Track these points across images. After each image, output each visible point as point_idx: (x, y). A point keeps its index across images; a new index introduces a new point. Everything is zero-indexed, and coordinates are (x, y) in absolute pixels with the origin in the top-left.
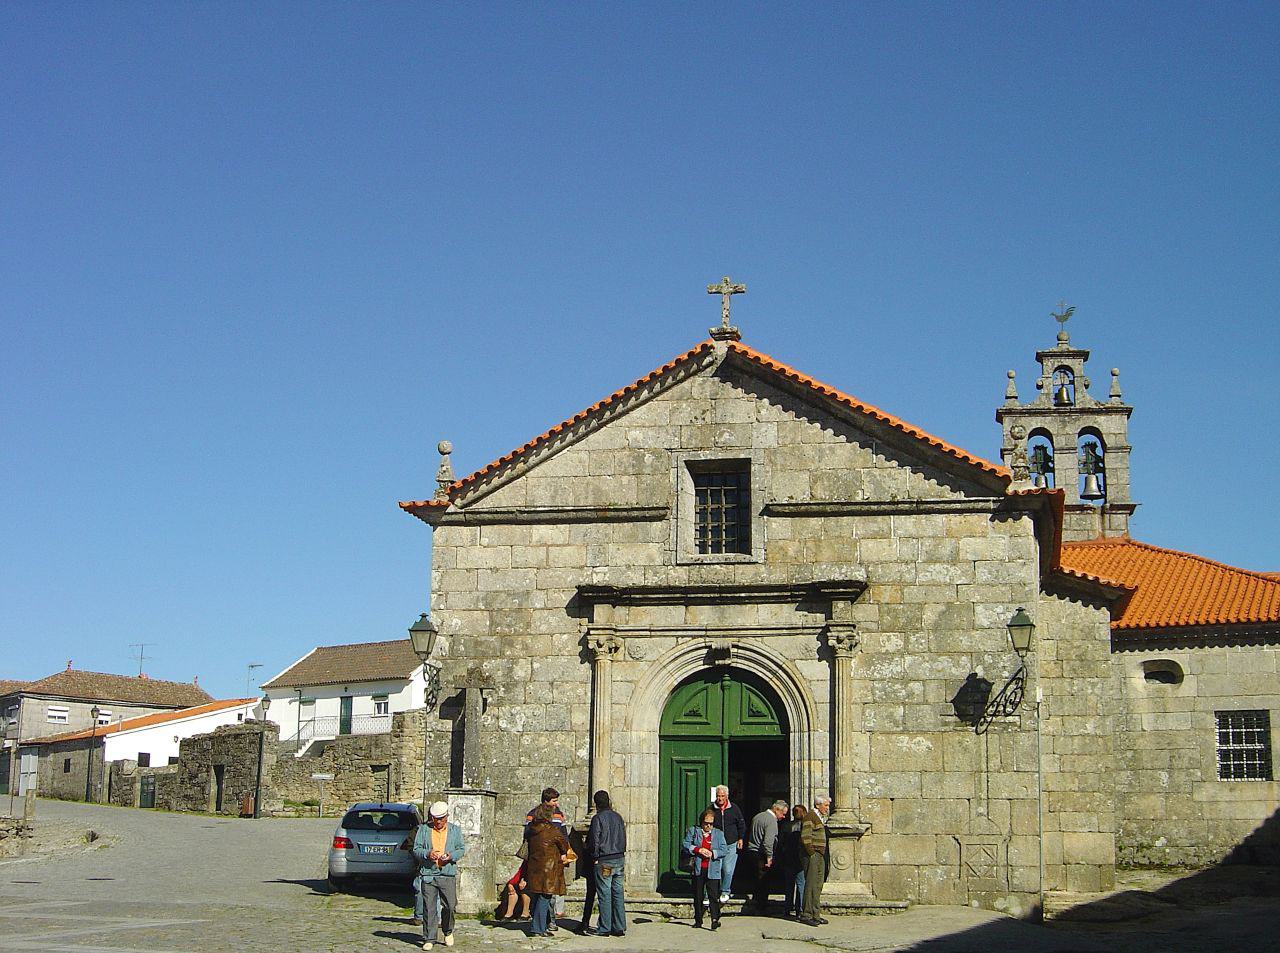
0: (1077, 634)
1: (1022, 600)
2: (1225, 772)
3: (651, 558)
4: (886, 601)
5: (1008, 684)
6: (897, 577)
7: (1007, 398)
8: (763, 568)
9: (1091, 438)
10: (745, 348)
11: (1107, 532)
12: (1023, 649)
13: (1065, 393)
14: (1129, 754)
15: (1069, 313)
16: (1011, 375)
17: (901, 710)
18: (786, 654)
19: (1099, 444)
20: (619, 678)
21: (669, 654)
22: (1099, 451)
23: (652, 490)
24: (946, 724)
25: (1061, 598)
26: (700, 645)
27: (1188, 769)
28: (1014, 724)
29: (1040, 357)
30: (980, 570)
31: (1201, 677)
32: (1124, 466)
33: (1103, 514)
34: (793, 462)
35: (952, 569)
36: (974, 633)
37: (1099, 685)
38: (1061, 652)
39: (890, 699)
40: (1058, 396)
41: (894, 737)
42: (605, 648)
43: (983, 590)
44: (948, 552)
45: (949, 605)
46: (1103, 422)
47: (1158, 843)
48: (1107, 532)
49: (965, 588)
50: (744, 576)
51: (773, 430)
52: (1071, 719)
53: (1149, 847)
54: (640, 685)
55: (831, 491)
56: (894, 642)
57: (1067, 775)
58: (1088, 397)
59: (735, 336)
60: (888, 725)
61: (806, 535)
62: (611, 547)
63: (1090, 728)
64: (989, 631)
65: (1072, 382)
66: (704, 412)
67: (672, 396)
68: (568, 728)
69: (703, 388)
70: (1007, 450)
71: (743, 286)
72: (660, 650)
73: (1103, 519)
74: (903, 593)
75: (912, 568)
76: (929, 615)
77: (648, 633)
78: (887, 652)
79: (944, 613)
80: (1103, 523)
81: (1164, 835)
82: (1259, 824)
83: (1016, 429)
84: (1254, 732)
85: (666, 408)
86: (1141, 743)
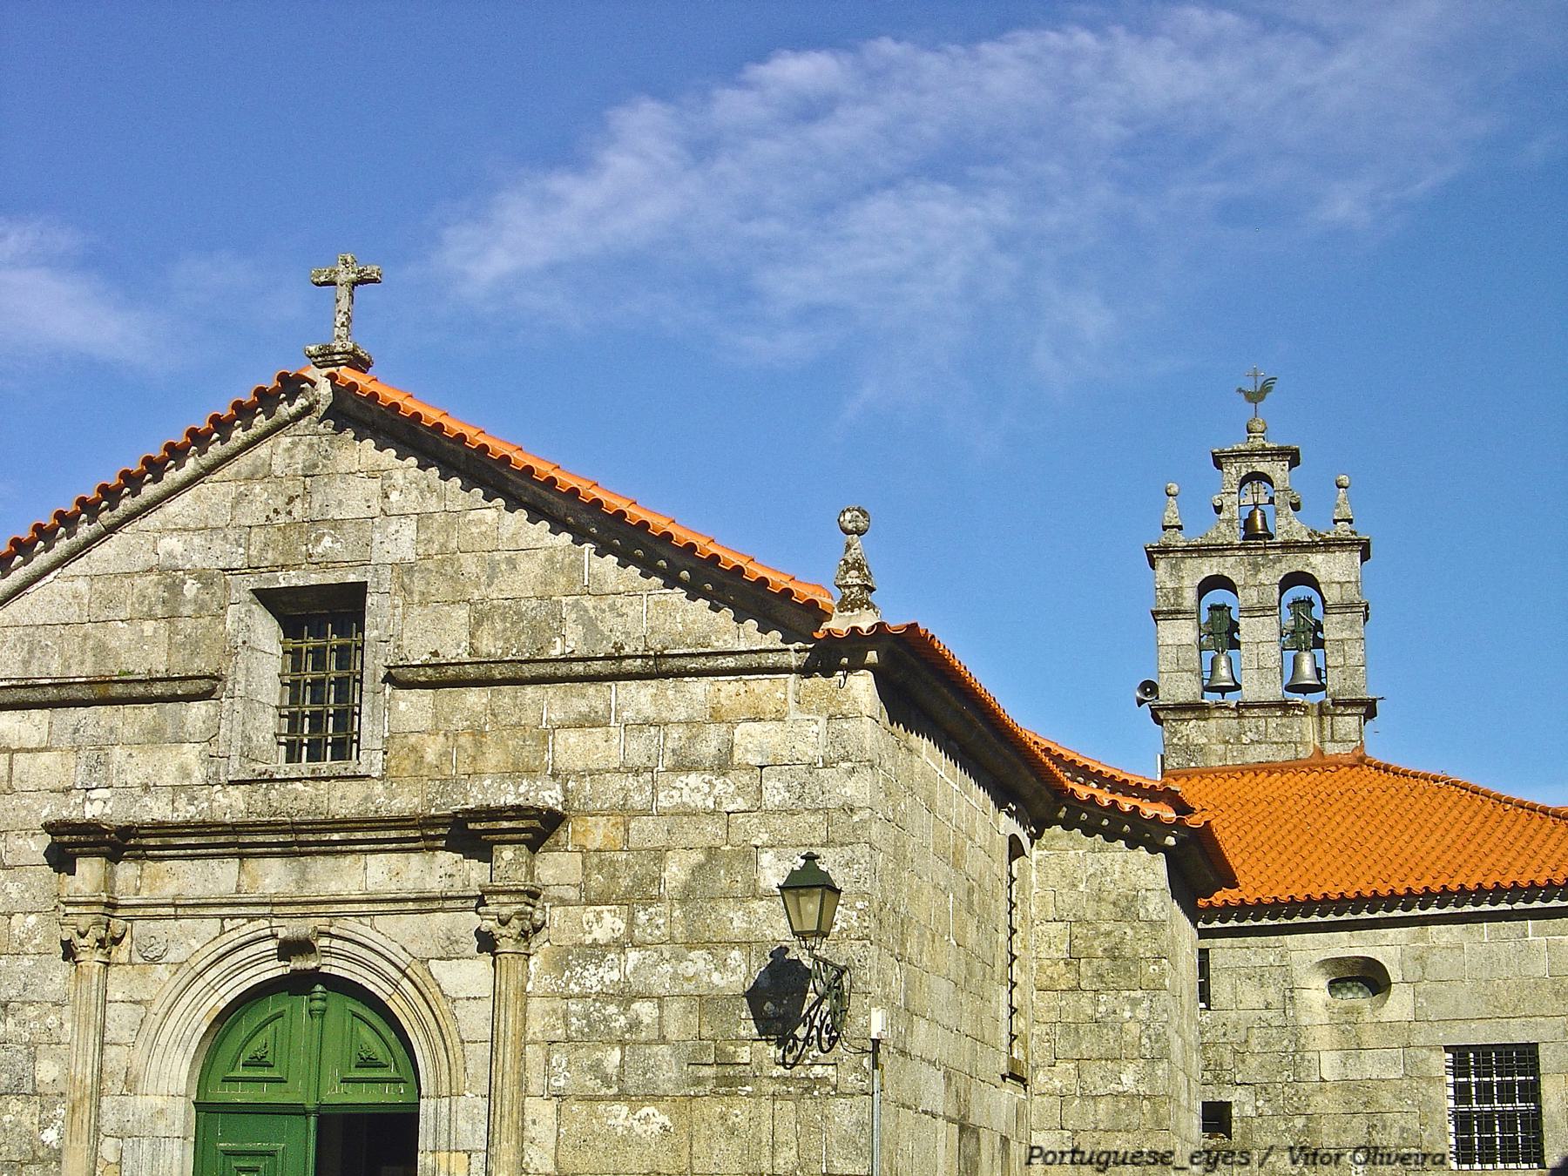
0: (1106, 910)
1: (848, 840)
3: (185, 772)
4: (596, 845)
6: (617, 799)
8: (379, 787)
10: (373, 387)
11: (1328, 746)
13: (1259, 518)
14: (1299, 1122)
15: (1266, 389)
16: (1171, 491)
17: (615, 1055)
18: (412, 948)
19: (1316, 599)
20: (119, 996)
21: (206, 951)
22: (1317, 612)
23: (194, 646)
24: (699, 1081)
26: (262, 933)
29: (1218, 461)
30: (770, 784)
31: (1421, 987)
32: (1355, 636)
34: (441, 589)
35: (719, 785)
36: (755, 904)
37: (1146, 1004)
38: (1077, 942)
39: (595, 1033)
40: (1249, 524)
41: (601, 1106)
42: (89, 940)
43: (777, 822)
44: (714, 751)
45: (712, 852)
46: (1320, 564)
48: (1328, 746)
49: (741, 818)
50: (344, 800)
51: (409, 530)
52: (1092, 1067)
54: (155, 1009)
55: (507, 640)
56: (608, 924)
58: (1296, 524)
59: (359, 363)
60: (592, 1084)
61: (459, 723)
62: (118, 754)
63: (1128, 1080)
65: (1272, 501)
66: (291, 500)
67: (238, 472)
68: (28, 1088)
69: (291, 457)
71: (372, 270)
72: (193, 942)
73: (1321, 720)
74: (627, 830)
75: (646, 782)
76: (675, 872)
77: (171, 911)
78: (595, 944)
79: (701, 866)
80: (1321, 729)
83: (848, 516)
85: (226, 494)
86: (1320, 1102)
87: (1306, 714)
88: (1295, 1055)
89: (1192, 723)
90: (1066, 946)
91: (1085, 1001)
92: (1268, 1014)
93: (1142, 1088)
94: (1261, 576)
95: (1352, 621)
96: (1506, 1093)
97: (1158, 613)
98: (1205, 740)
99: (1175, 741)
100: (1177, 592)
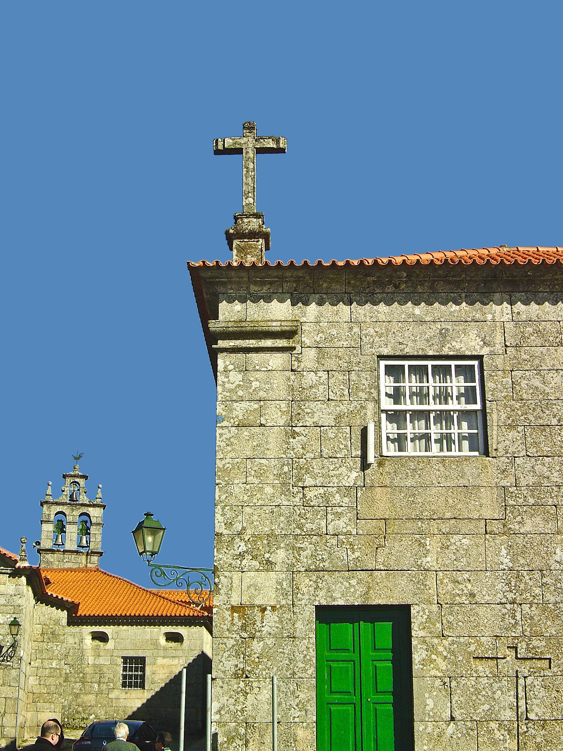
0: (52, 622)
2: (124, 685)
5: (9, 648)
7: (47, 495)
9: (85, 518)
12: (15, 635)
14: (81, 675)
15: (80, 457)
16: (50, 484)
22: (88, 524)
25: (47, 605)
27: (107, 683)
28: (10, 665)
31: (116, 640)
32: (99, 533)
33: (87, 555)
37: (60, 646)
40: (71, 496)
46: (92, 511)
47: (91, 717)
52: (46, 661)
53: (87, 719)
57: (42, 686)
58: (86, 498)
63: (54, 665)
64: (3, 625)
65: (79, 490)
70: (44, 521)
80: (87, 560)
81: (94, 713)
82: (135, 709)
83: (23, 539)
84: (138, 667)
86: (87, 670)
87: (83, 555)
88: (82, 657)
89: (50, 555)
90: (41, 631)
91: (45, 644)
92: (75, 646)
93: (57, 667)
94: (74, 513)
95: (99, 528)
96: (136, 669)
97: (43, 521)
98: (53, 560)
99: (44, 560)
100: (49, 515)
